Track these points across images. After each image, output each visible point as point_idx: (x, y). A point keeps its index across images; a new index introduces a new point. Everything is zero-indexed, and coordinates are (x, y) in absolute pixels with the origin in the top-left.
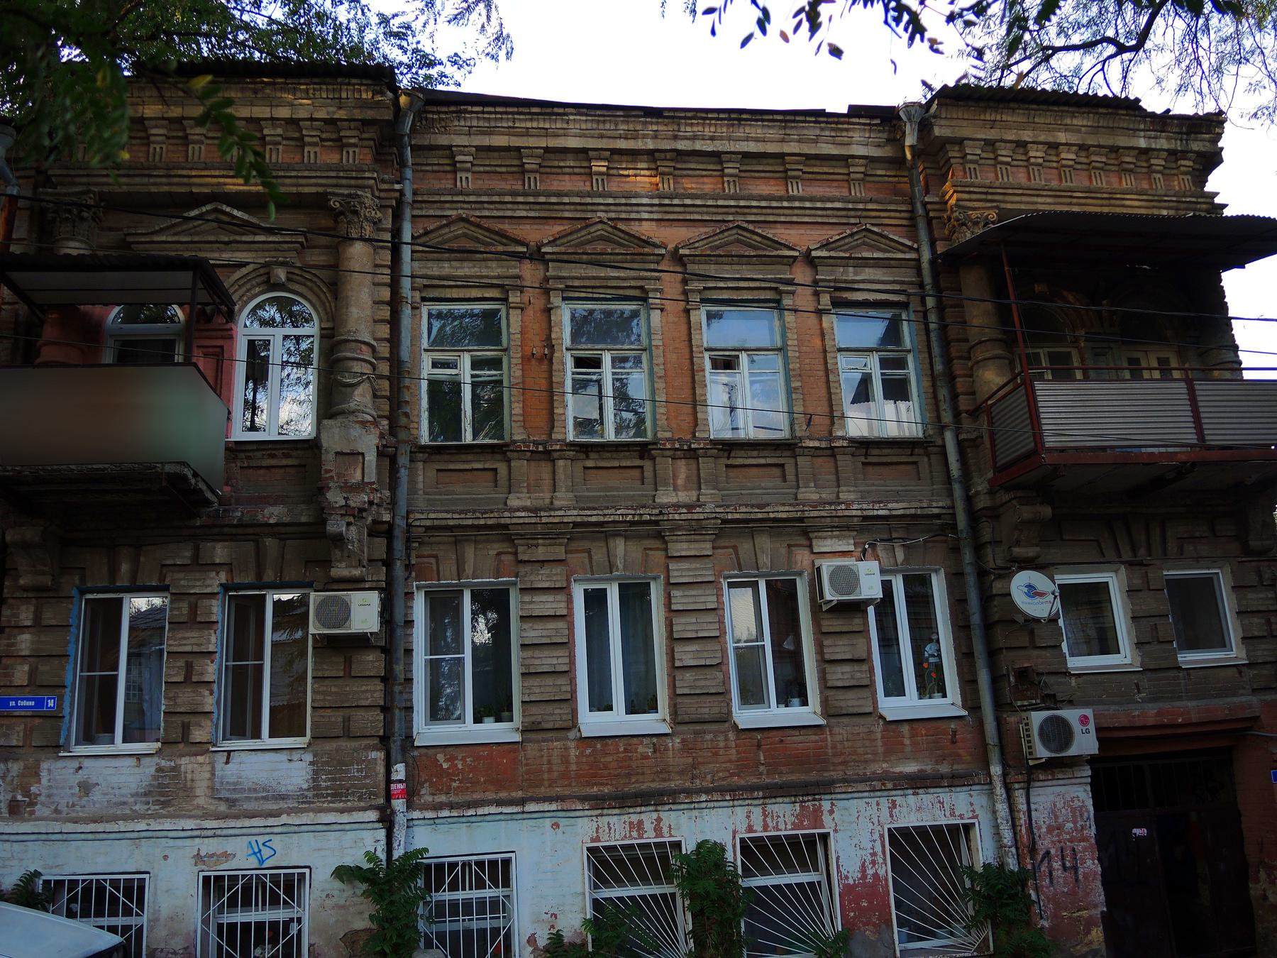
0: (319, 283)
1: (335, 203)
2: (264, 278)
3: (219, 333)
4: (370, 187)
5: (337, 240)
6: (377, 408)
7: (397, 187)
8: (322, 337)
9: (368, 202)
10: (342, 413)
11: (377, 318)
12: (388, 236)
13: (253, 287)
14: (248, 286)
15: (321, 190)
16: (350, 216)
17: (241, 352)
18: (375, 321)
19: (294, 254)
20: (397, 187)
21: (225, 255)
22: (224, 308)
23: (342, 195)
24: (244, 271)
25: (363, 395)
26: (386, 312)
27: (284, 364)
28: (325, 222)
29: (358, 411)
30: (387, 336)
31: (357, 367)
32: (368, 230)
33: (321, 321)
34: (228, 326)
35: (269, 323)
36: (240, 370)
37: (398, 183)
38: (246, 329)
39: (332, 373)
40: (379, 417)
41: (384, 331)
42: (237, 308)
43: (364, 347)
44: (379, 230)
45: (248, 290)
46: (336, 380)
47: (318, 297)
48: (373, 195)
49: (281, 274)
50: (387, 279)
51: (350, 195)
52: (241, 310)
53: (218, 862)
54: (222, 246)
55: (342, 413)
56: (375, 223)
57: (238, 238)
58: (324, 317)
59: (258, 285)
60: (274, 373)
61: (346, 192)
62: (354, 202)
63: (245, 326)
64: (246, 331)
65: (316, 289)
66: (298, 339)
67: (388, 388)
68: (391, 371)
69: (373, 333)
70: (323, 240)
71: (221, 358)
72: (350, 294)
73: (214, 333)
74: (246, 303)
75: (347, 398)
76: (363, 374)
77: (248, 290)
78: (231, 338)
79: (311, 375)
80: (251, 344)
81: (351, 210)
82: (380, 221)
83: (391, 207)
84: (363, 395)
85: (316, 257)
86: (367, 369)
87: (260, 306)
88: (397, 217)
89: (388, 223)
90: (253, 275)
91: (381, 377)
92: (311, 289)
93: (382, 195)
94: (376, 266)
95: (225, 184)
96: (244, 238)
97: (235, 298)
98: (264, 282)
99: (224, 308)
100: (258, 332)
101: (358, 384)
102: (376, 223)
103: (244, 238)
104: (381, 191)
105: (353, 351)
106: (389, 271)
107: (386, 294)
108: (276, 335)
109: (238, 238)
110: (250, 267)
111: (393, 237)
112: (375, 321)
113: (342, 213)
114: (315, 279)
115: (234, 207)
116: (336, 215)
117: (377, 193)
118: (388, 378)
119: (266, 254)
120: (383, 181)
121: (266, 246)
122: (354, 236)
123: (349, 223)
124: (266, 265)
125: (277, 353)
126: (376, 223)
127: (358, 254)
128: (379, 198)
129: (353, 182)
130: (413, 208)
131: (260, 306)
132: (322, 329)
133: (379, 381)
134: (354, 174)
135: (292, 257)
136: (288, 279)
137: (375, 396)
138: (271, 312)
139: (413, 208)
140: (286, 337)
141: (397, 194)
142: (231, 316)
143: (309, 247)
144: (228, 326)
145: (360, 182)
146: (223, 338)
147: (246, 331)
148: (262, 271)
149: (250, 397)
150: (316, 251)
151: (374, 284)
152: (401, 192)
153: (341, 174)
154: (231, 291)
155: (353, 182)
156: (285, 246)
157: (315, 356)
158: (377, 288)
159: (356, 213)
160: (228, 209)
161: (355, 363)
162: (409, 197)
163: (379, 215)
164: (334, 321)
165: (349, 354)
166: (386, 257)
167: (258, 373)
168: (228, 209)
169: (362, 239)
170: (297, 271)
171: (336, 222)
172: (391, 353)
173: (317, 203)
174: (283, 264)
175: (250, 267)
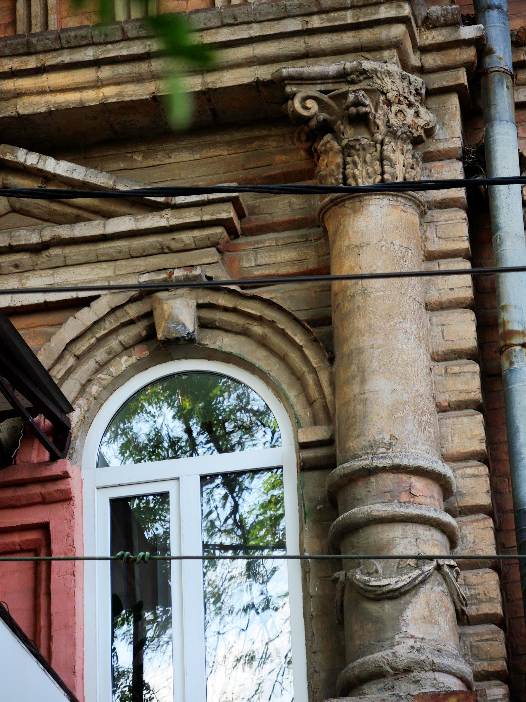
0: (283, 323)
1: (304, 104)
2: (138, 330)
3: (36, 490)
4: (396, 45)
5: (318, 201)
6: (471, 653)
7: (468, 32)
8: (304, 467)
9: (393, 86)
10: (377, 675)
11: (444, 399)
12: (455, 170)
13: (114, 356)
14: (101, 355)
15: (264, 73)
16: (349, 134)
17: (93, 531)
18: (442, 409)
19: (211, 255)
20: (468, 32)
21: (35, 281)
22: (42, 421)
23: (323, 78)
24: (86, 317)
25: (429, 620)
26: (468, 381)
27: (210, 555)
28: (281, 156)
29: (421, 666)
30: (477, 395)
31: (407, 541)
32: (401, 163)
33: (297, 424)
34: (56, 469)
35: (155, 448)
36: (94, 587)
37: (470, 21)
38: (99, 472)
39: (338, 564)
40: (482, 676)
41: (470, 433)
42: (75, 417)
43: (419, 484)
44: (429, 158)
45: (101, 367)
46: (351, 583)
47: (283, 359)
48: (405, 65)
49: (180, 312)
50: (462, 287)
51: (342, 77)
52: (87, 422)
53: (415, 581)
54: (24, 258)
55: (377, 675)
56: (416, 142)
57: (64, 232)
58: (304, 414)
59: (126, 348)
60: (186, 581)
61: (331, 67)
62: (354, 92)
63: (102, 463)
64: (104, 476)
65: (276, 340)
66: (232, 481)
67: (495, 593)
68: (500, 545)
69: (440, 441)
70: (283, 207)
71: (40, 553)
72: (366, 342)
73: (22, 492)
74: (99, 402)
75: (383, 633)
76: (422, 559)
77: (101, 367)
78: (66, 498)
79: (284, 578)
80: (120, 508)
81: (350, 114)
82: (429, 132)
83: (457, 89)
84: (429, 620)
85: (269, 256)
86: (432, 543)
87: (128, 410)
88: (476, 114)
89: (451, 135)
90: (109, 325)
91: (473, 563)
92: (262, 343)
93: (431, 60)
94: (431, 257)
95: (19, 94)
96: (82, 230)
97: (69, 390)
98: (141, 341)
99: (42, 421)
100: (140, 478)
101: (413, 588)
102: (419, 140)
103: (82, 230)
104: (424, 50)
105: (391, 496)
106: (467, 265)
107: (463, 330)
108: (182, 479)
109: (64, 232)
110: (101, 307)
111: (468, 170)
112: (442, 409)
113: (326, 127)
114: (270, 314)
115: (58, 154)
116: (310, 133)
117: (415, 60)
118: (495, 565)
119: (141, 264)
120: (429, 23)
121: (137, 243)
122: (363, 182)
123: (347, 150)
124: (146, 292)
125: (185, 528)
126: (419, 140)
127: (378, 232)
128: (421, 71)
129: (348, 39)
130: (517, 84)
131: (128, 410)
132: (303, 446)
133: (471, 576)
134: (349, 17)
135: (208, 264)
136: (204, 325)
137: (462, 618)
138: (166, 420)
139: (517, 84)
140: (206, 479)
141: (469, 54)
142: (60, 441)
143: (250, 232)
144: (56, 469)
145: (366, 36)
146: (45, 501)
147: (104, 476)
148: (133, 311)
149: (126, 661)
150: (269, 238)
151: (432, 307)
152: (481, 46)
153: (316, 22)
154: (57, 374)
155: (348, 39)
156: (187, 237)
157: (290, 525)
158: (439, 317)
159: (362, 121)
160: (31, 159)
161: (396, 532)
162: (502, 55)
163: (426, 117)
164: (330, 419)
165: (379, 509)
166: (454, 229)
167: (141, 590)
168: (31, 159)
169: (384, 188)
170: (222, 300)
171: (313, 155)
172: (495, 491)
173: (252, 113)
174: (190, 284)
175: (101, 307)
